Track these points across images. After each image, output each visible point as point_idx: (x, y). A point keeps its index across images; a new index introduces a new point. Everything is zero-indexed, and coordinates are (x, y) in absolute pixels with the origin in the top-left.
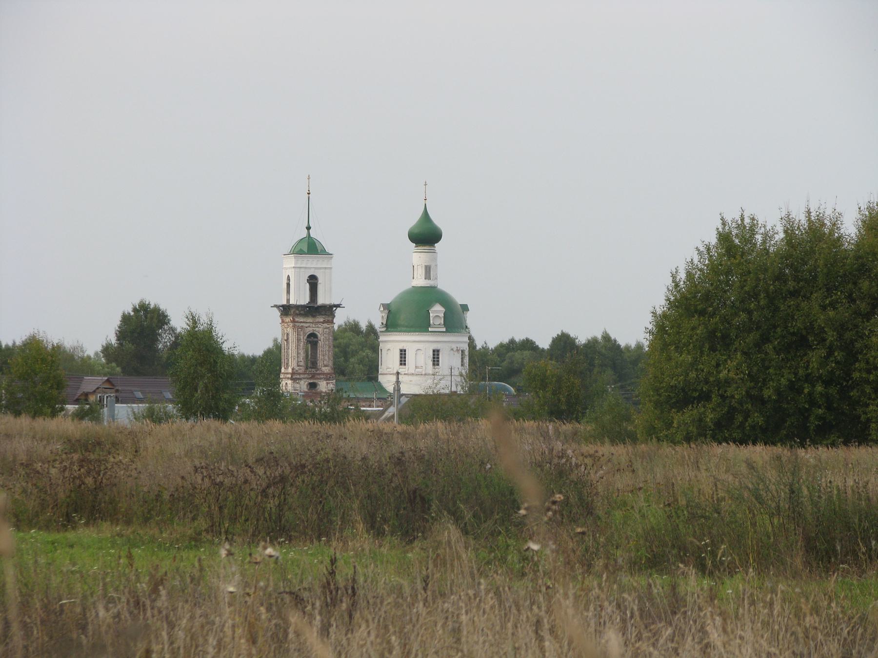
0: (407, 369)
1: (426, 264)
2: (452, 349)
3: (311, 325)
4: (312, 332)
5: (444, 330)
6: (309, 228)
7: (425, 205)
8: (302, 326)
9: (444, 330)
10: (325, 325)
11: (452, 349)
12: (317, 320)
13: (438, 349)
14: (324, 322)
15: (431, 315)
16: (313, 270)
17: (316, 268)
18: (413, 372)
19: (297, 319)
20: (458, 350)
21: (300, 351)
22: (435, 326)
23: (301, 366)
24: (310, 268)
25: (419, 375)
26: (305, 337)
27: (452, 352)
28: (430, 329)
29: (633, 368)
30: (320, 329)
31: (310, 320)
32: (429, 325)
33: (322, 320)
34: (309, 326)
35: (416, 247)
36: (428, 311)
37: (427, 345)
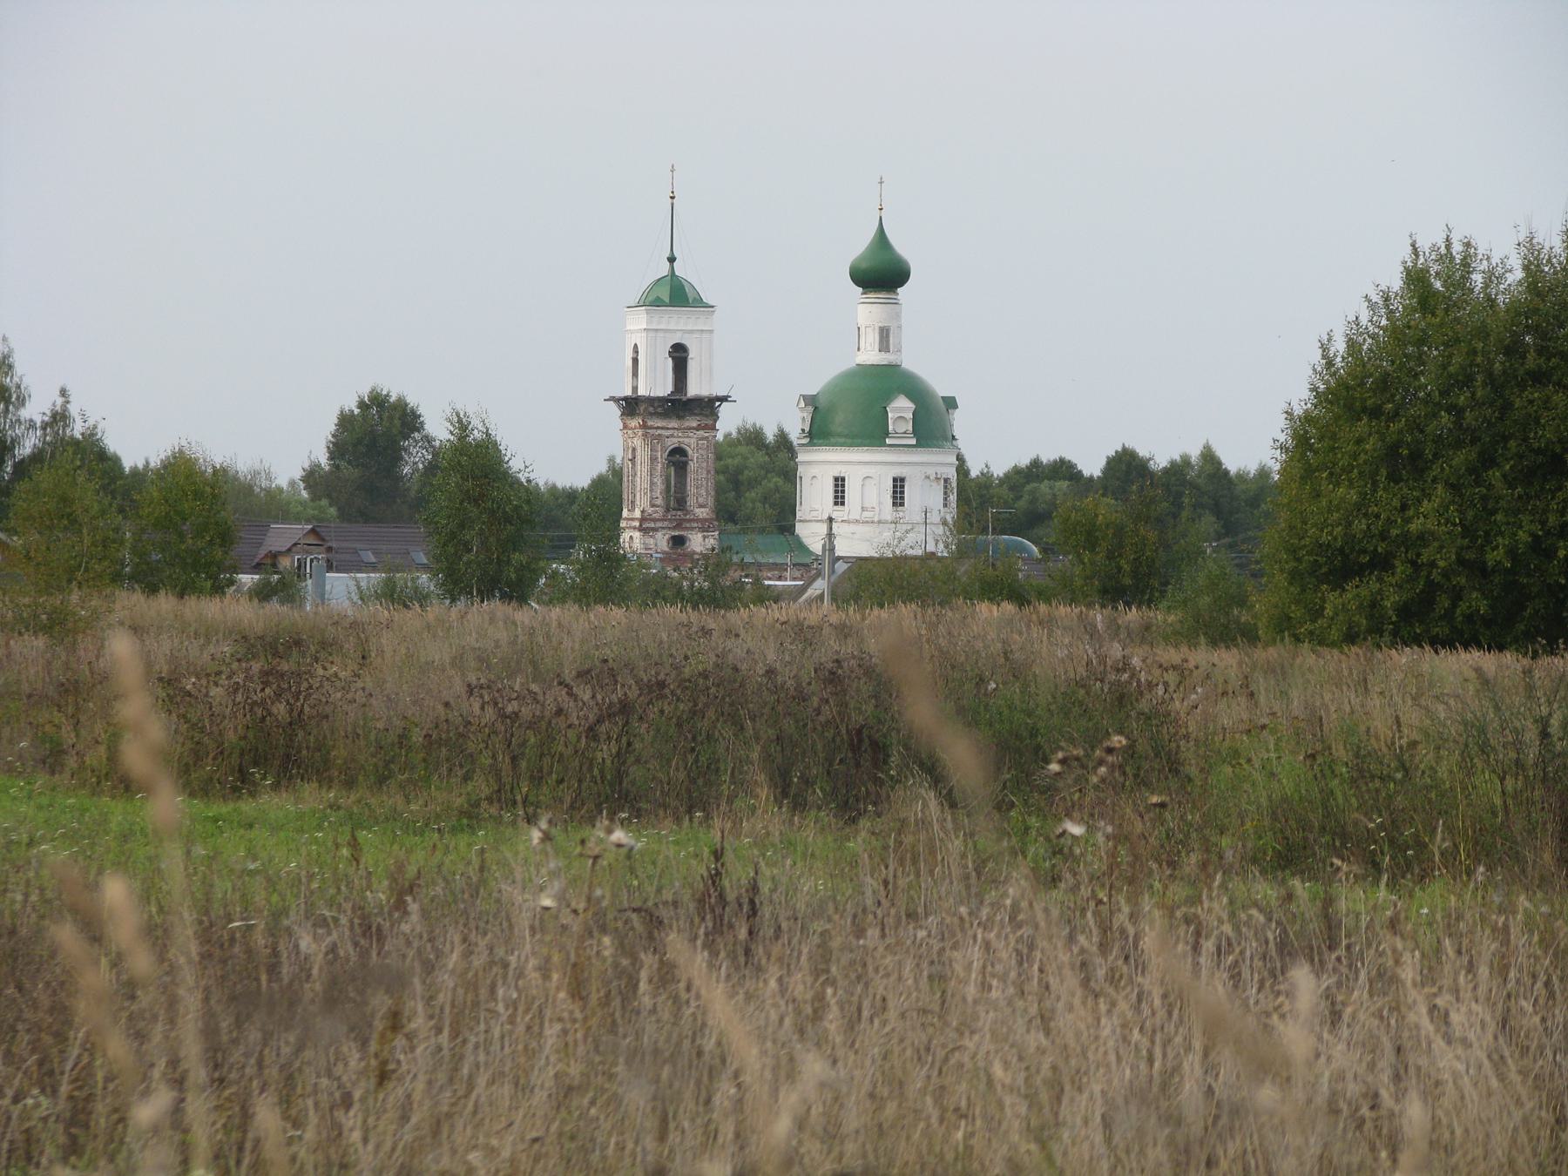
2: (928, 477)
6: (672, 260)
9: (913, 442)
11: (928, 477)
14: (698, 428)
16: (679, 334)
17: (684, 331)
19: (650, 423)
27: (927, 481)
28: (888, 441)
30: (692, 441)
31: (674, 424)
32: (887, 434)
34: (672, 436)
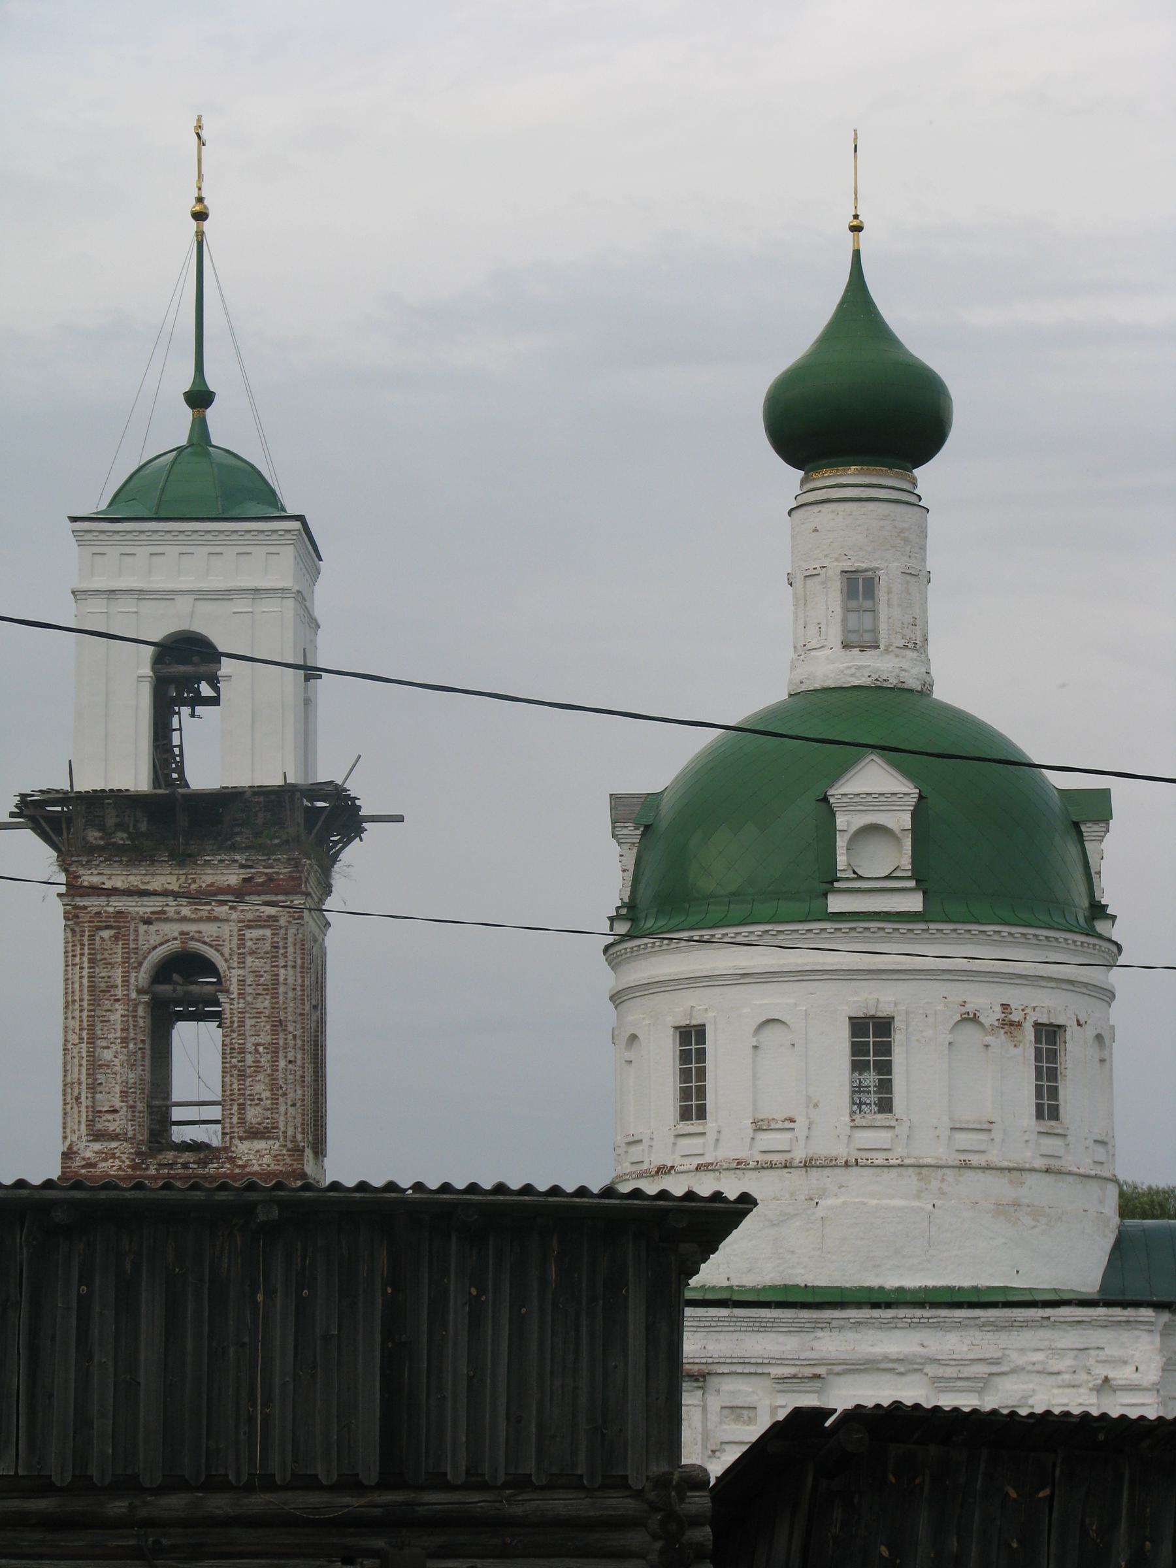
0: (711, 1137)
1: (847, 565)
2: (971, 1019)
3: (170, 907)
4: (175, 945)
5: (914, 903)
6: (200, 398)
7: (857, 254)
8: (120, 914)
9: (914, 903)
10: (256, 907)
11: (971, 1019)
12: (208, 878)
13: (884, 1011)
14: (239, 894)
15: (841, 821)
16: (184, 604)
17: (202, 595)
18: (742, 1154)
19: (89, 878)
20: (1010, 1025)
21: (107, 1055)
22: (860, 884)
23: (115, 1137)
24: (168, 595)
25: (771, 1166)
26: (142, 977)
27: (971, 1033)
28: (835, 904)
29: (729, 1267)
30: (226, 930)
31: (165, 878)
32: (829, 880)
33: (233, 878)
34: (160, 917)
35: (804, 481)
36: (825, 799)
37: (825, 991)
